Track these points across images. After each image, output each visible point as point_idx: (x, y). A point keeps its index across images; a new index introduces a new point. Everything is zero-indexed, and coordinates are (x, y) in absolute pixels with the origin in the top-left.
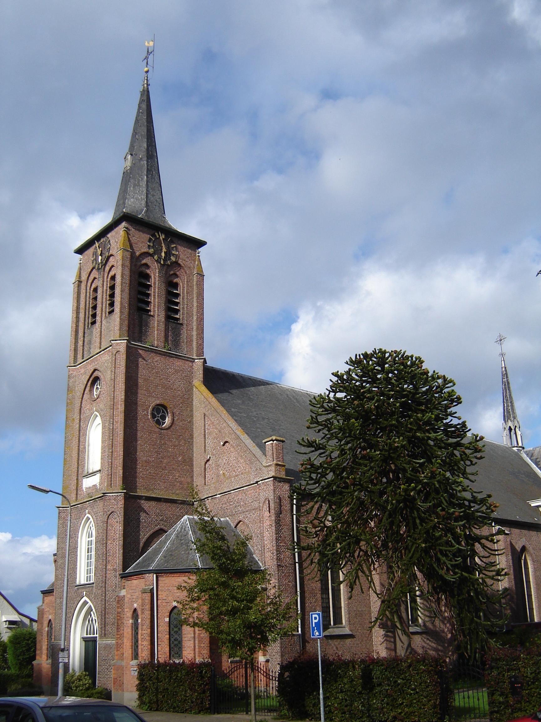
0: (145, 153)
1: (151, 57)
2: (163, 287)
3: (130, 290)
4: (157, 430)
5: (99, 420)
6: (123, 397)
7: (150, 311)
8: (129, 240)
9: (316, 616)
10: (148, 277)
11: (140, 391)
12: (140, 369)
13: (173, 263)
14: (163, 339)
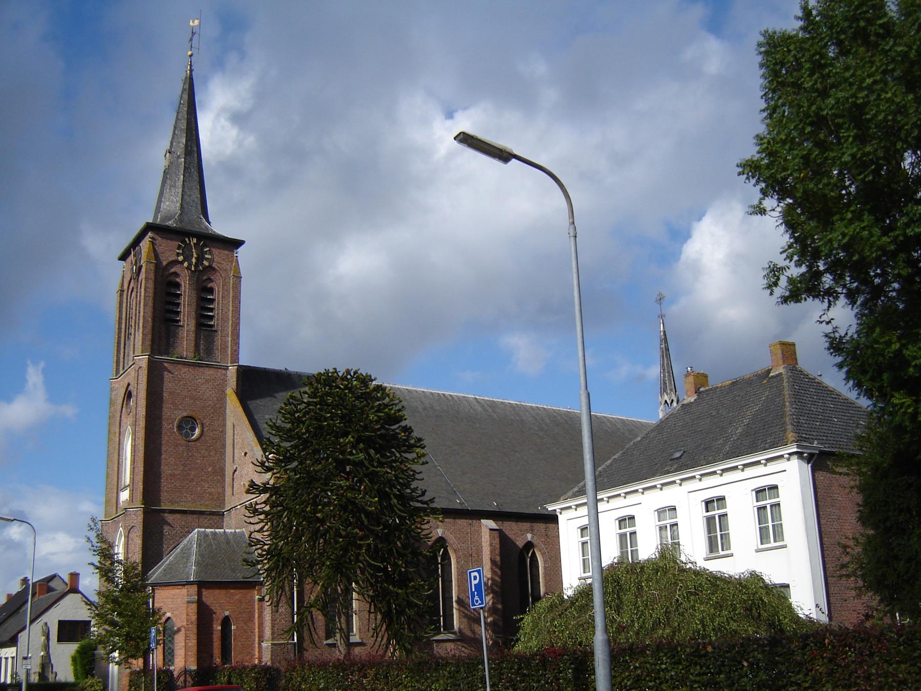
0: (183, 150)
1: (196, 36)
2: (194, 295)
3: (154, 303)
4: (183, 442)
6: (144, 413)
7: (179, 321)
8: (155, 250)
9: (476, 574)
10: (178, 286)
11: (164, 405)
12: (165, 383)
13: (205, 268)
14: (192, 349)
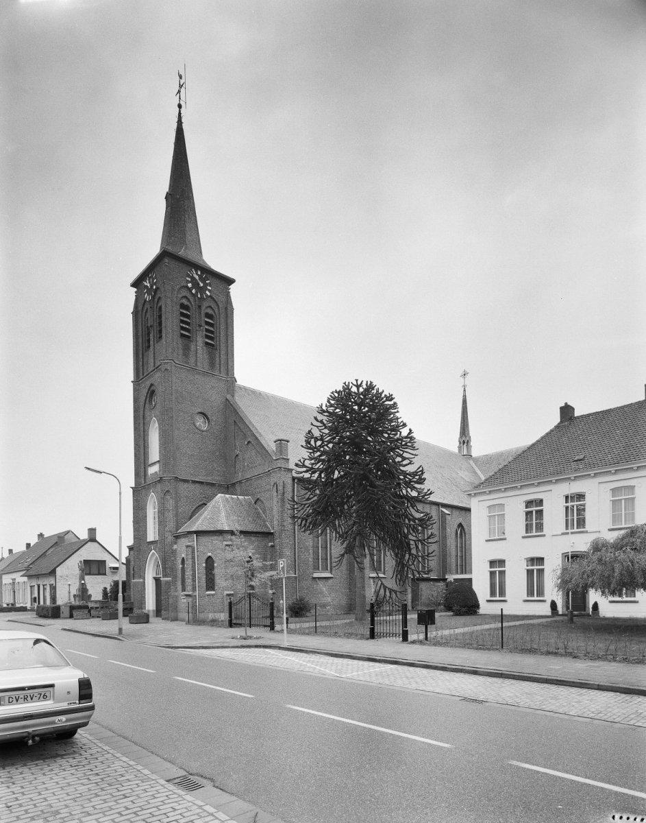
1: (183, 90)
5: (157, 425)
